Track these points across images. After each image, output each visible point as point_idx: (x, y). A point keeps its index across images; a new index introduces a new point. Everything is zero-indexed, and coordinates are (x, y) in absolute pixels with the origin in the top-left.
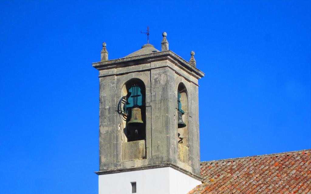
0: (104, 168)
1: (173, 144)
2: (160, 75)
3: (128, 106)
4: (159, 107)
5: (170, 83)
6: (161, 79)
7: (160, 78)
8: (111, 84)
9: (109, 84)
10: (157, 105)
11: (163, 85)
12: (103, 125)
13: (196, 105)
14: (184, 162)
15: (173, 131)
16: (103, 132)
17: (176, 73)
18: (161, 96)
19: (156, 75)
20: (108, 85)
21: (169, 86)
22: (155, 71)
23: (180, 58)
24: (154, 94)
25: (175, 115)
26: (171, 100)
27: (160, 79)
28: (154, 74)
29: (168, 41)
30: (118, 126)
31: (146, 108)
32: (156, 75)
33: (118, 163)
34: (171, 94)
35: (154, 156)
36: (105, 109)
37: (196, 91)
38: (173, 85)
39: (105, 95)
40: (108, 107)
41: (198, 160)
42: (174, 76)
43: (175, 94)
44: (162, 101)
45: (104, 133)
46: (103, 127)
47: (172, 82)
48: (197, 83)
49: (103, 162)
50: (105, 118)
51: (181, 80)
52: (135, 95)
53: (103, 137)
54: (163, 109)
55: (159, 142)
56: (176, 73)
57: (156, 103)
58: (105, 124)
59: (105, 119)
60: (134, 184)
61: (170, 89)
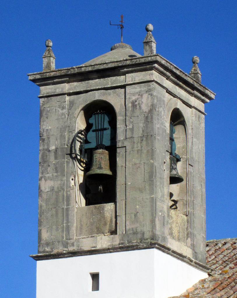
1: (161, 211)
2: (142, 96)
4: (139, 148)
5: (157, 109)
6: (142, 102)
7: (141, 101)
8: (60, 110)
9: (56, 110)
10: (136, 146)
11: (146, 112)
15: (162, 189)
16: (46, 189)
18: (143, 131)
19: (134, 94)
20: (54, 110)
21: (156, 114)
22: (134, 88)
23: (175, 68)
24: (131, 127)
25: (165, 163)
27: (140, 102)
28: (131, 94)
30: (71, 180)
32: (134, 94)
33: (69, 241)
34: (158, 128)
36: (49, 151)
37: (200, 123)
38: (163, 113)
39: (50, 127)
40: (53, 148)
41: (203, 237)
44: (144, 139)
45: (47, 190)
46: (46, 180)
47: (161, 107)
48: (203, 110)
50: (49, 166)
53: (45, 197)
58: (48, 175)
59: (49, 168)
60: (95, 277)
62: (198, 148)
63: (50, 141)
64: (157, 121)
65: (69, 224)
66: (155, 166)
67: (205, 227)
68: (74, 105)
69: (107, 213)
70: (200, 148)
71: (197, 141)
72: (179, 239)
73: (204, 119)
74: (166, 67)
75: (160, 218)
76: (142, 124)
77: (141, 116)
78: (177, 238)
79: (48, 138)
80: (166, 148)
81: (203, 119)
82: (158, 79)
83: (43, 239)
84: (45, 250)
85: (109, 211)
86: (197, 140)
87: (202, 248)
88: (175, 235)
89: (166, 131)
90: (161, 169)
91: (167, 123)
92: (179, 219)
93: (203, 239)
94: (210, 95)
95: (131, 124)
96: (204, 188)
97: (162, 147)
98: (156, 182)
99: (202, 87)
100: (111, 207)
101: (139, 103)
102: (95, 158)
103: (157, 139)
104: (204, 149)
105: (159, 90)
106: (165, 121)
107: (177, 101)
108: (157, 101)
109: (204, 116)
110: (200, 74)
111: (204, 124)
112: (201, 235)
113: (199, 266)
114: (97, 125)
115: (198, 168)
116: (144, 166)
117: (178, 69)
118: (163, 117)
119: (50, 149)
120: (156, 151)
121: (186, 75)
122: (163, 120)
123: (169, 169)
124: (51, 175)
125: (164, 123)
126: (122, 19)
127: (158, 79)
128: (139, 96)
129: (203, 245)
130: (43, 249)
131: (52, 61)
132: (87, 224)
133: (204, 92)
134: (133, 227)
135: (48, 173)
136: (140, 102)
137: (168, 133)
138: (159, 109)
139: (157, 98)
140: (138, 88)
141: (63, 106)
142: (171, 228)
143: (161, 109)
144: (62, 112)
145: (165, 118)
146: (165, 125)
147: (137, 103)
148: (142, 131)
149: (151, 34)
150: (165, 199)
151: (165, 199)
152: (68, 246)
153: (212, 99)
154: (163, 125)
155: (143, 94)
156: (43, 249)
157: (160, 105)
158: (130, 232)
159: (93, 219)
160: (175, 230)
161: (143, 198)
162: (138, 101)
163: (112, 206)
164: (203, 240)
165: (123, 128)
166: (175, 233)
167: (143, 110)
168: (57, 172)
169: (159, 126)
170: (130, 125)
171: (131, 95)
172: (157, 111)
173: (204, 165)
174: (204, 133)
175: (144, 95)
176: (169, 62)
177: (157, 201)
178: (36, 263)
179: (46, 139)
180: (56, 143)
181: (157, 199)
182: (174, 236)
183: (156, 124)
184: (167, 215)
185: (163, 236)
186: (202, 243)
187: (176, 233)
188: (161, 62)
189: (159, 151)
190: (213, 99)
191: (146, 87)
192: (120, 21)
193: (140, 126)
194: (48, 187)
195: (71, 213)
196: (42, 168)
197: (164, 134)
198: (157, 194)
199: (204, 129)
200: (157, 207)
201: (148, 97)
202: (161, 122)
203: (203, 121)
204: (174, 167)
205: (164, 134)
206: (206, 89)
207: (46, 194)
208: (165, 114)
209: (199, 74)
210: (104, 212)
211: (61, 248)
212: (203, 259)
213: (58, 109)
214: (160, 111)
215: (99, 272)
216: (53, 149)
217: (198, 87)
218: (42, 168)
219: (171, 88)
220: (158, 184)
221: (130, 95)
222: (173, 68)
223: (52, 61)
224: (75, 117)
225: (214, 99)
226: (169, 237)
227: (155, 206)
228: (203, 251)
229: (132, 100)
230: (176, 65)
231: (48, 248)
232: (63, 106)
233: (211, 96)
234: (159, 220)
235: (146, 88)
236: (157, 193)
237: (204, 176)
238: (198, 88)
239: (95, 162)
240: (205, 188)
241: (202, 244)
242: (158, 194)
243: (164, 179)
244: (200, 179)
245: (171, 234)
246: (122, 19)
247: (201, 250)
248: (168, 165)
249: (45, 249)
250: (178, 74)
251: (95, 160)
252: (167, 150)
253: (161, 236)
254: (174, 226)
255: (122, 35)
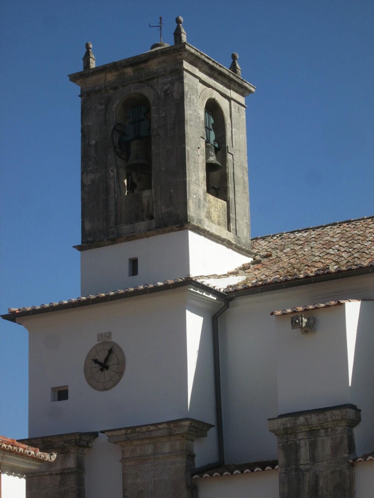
0: (89, 239)
1: (195, 194)
5: (189, 96)
9: (95, 106)
14: (219, 224)
15: (196, 172)
20: (94, 107)
21: (188, 101)
24: (164, 115)
25: (199, 148)
26: (192, 123)
27: (172, 90)
29: (185, 30)
30: (110, 171)
31: (152, 138)
34: (190, 114)
36: (90, 146)
37: (240, 115)
38: (195, 100)
39: (90, 124)
42: (197, 86)
43: (199, 114)
45: (89, 183)
46: (87, 174)
47: (193, 94)
50: (90, 160)
51: (212, 94)
55: (172, 191)
58: (89, 169)
61: (190, 106)
62: (239, 137)
66: (188, 151)
67: (249, 214)
70: (241, 138)
71: (237, 131)
73: (244, 111)
74: (197, 55)
75: (194, 200)
78: (217, 222)
81: (243, 111)
82: (189, 67)
87: (246, 233)
88: (215, 219)
89: (199, 118)
90: (195, 154)
91: (201, 111)
99: (240, 80)
100: (148, 193)
104: (246, 140)
105: (190, 78)
106: (198, 109)
109: (244, 109)
117: (210, 60)
118: (196, 105)
119: (91, 144)
121: (220, 66)
122: (196, 107)
123: (204, 154)
125: (197, 110)
126: (161, 21)
127: (189, 67)
128: (171, 86)
133: (242, 85)
138: (192, 97)
142: (210, 212)
143: (193, 97)
144: (100, 108)
145: (199, 105)
146: (199, 112)
147: (168, 92)
150: (200, 183)
151: (200, 183)
157: (192, 93)
162: (170, 90)
166: (214, 217)
169: (191, 113)
173: (246, 154)
177: (190, 184)
180: (96, 137)
181: (190, 182)
182: (213, 220)
183: (187, 110)
184: (203, 198)
185: (199, 219)
190: (253, 92)
195: (301, 422)
199: (245, 120)
200: (191, 190)
204: (211, 154)
208: (198, 102)
209: (239, 69)
219: (205, 78)
220: (192, 167)
225: (255, 92)
226: (206, 220)
230: (208, 55)
234: (193, 202)
236: (190, 176)
238: (235, 80)
240: (247, 177)
241: (246, 229)
246: (161, 21)
247: (245, 235)
248: (204, 151)
252: (201, 136)
253: (196, 218)
254: (212, 210)
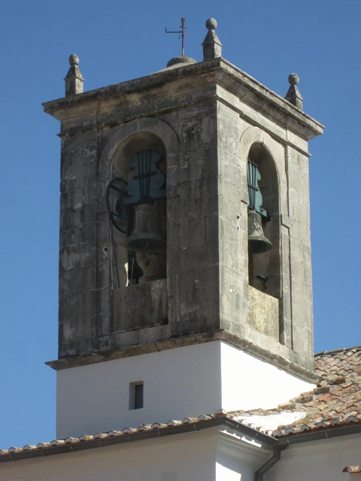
0: (70, 352)
1: (232, 287)
2: (201, 120)
3: (127, 201)
4: (198, 196)
6: (202, 130)
7: (200, 128)
8: (88, 151)
9: (82, 151)
10: (193, 192)
11: (206, 143)
12: (68, 248)
13: (301, 201)
16: (69, 265)
17: (244, 117)
18: (203, 171)
19: (190, 119)
20: (80, 153)
22: (190, 111)
23: (252, 81)
24: (186, 166)
25: (238, 217)
26: (228, 180)
27: (199, 130)
28: (186, 119)
30: (103, 250)
32: (190, 119)
33: (101, 339)
34: (226, 166)
35: (185, 315)
36: (74, 211)
37: (300, 168)
38: (234, 145)
39: (74, 177)
40: (78, 206)
41: (309, 331)
43: (239, 165)
44: (205, 182)
46: (69, 253)
47: (231, 136)
48: (306, 149)
49: (67, 338)
50: (73, 232)
52: (145, 172)
53: (68, 278)
54: (206, 200)
55: (196, 281)
56: (244, 117)
57: (190, 189)
58: (71, 246)
59: (73, 235)
60: (137, 390)
62: (298, 202)
63: (74, 197)
64: (224, 155)
65: (101, 314)
68: (108, 142)
69: (155, 294)
70: (302, 202)
72: (267, 332)
73: (307, 161)
75: (230, 296)
76: (201, 161)
77: (201, 149)
78: (263, 329)
79: (73, 193)
80: (240, 197)
81: (305, 162)
82: (225, 95)
83: (65, 339)
84: (69, 353)
85: (157, 291)
86: (296, 190)
89: (239, 172)
90: (232, 226)
92: (266, 302)
93: (309, 334)
94: (314, 127)
95: (186, 163)
96: (308, 261)
97: (234, 194)
98: (223, 243)
99: (301, 115)
101: (197, 132)
102: (137, 217)
103: (224, 181)
107: (260, 131)
108: (224, 127)
109: (307, 158)
110: (301, 98)
111: (308, 170)
112: (305, 328)
113: (295, 371)
114: (141, 169)
115: (299, 231)
116: (205, 221)
117: (257, 84)
118: (234, 152)
119: (74, 208)
120: (222, 198)
121: (271, 94)
122: (235, 155)
123: (246, 227)
124: (76, 245)
127: (225, 95)
128: (197, 122)
129: (309, 342)
130: (66, 352)
131: (78, 84)
132: (126, 313)
134: (190, 311)
135: (72, 243)
136: (198, 129)
137: (244, 176)
138: (228, 140)
139: (224, 123)
140: (196, 110)
141: (93, 145)
143: (230, 140)
144: (90, 154)
146: (239, 164)
147: (194, 132)
148: (201, 171)
149: (215, 32)
151: (240, 270)
152: (100, 345)
153: (319, 135)
154: (234, 163)
155: (203, 118)
156: (66, 352)
157: (228, 134)
158: (187, 319)
159: (135, 305)
160: (259, 318)
161: (204, 268)
162: (195, 128)
163: (161, 284)
164: (308, 336)
165: (175, 168)
166: (259, 322)
167: (203, 141)
168: (84, 240)
169: (227, 164)
170: (185, 164)
171: (186, 120)
172: (224, 142)
174: (308, 182)
175: (204, 118)
176: (241, 71)
177: (225, 272)
178: (240, 473)
179: (69, 195)
181: (225, 268)
186: (306, 339)
187: (261, 323)
188: (227, 70)
189: (228, 200)
190: (321, 134)
191: (206, 108)
192: (180, 27)
193: (199, 163)
194: (72, 263)
196: (64, 236)
197: (237, 175)
198: (225, 262)
200: (225, 281)
201: (210, 121)
202: (230, 158)
203: (305, 165)
204: (257, 227)
205: (237, 175)
206: (308, 118)
207: (68, 273)
210: (151, 293)
211: (90, 350)
212: (308, 362)
213: (86, 150)
214: (229, 142)
215: (142, 382)
216: (79, 208)
217: (293, 114)
218: (64, 236)
221: (184, 121)
222: (247, 81)
223: (78, 84)
224: (109, 160)
225: (323, 133)
226: (247, 326)
227: (222, 278)
228: (309, 351)
229: (187, 127)
231: (72, 351)
232: (93, 145)
233: (316, 129)
235: (207, 109)
237: (308, 244)
238: (294, 115)
239: (137, 222)
242: (227, 262)
243: (237, 240)
244: (302, 247)
245: (252, 321)
247: (305, 350)
248: (245, 221)
249: (68, 353)
250: (258, 90)
251: (137, 219)
253: (233, 323)
254: (257, 311)
255: (183, 46)
